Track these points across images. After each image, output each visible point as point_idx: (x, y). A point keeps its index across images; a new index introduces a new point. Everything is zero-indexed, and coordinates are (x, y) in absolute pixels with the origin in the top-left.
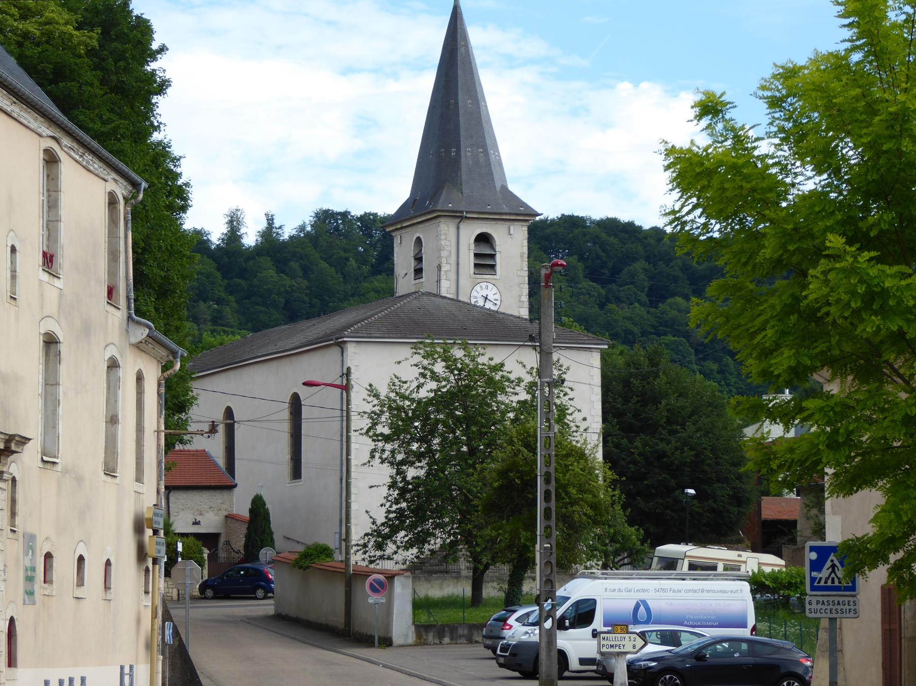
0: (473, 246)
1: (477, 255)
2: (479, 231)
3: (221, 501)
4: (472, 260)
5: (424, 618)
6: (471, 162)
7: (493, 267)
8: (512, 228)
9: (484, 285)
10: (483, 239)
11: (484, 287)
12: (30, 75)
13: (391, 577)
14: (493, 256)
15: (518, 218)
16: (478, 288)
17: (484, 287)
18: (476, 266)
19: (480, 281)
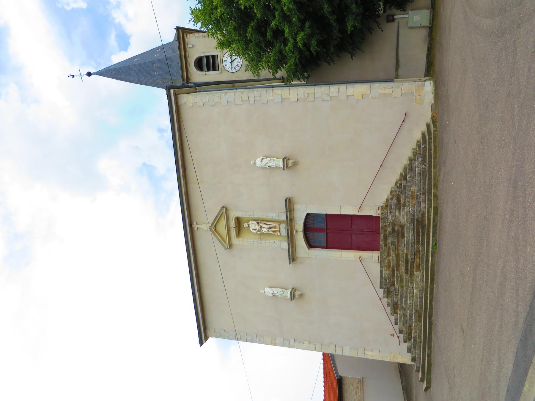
0: (203, 72)
1: (208, 70)
2: (194, 69)
3: (351, 386)
4: (211, 72)
5: (205, 68)
6: (161, 72)
7: (214, 57)
8: (189, 46)
9: (225, 63)
10: (199, 64)
11: (225, 63)
12: (528, 372)
13: (405, 310)
14: (207, 57)
15: (182, 43)
16: (226, 68)
17: (225, 63)
18: (214, 70)
19: (222, 66)
